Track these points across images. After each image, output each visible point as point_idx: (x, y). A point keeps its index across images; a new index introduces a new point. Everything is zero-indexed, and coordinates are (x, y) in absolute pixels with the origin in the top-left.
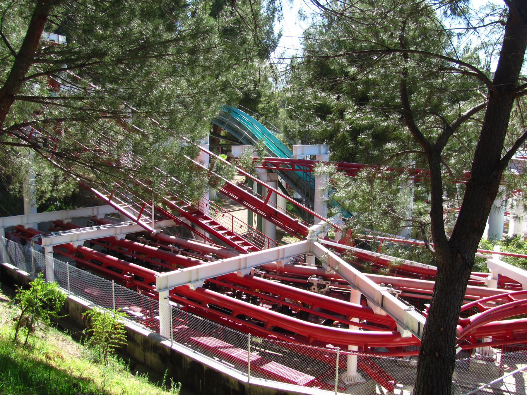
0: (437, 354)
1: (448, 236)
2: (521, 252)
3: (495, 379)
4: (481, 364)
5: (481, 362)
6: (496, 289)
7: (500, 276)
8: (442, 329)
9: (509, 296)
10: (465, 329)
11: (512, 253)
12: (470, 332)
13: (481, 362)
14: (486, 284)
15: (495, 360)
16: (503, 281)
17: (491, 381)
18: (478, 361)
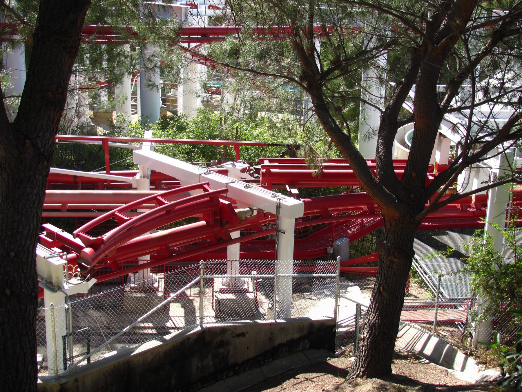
0: (8, 292)
1: (12, 116)
2: (183, 137)
3: (144, 314)
4: (137, 298)
5: (139, 295)
6: (146, 191)
7: (153, 172)
8: (12, 254)
9: (159, 198)
10: (98, 252)
11: (170, 139)
12: (107, 256)
13: (139, 295)
14: (134, 186)
15: (157, 289)
16: (157, 179)
17: (138, 318)
18: (135, 295)
